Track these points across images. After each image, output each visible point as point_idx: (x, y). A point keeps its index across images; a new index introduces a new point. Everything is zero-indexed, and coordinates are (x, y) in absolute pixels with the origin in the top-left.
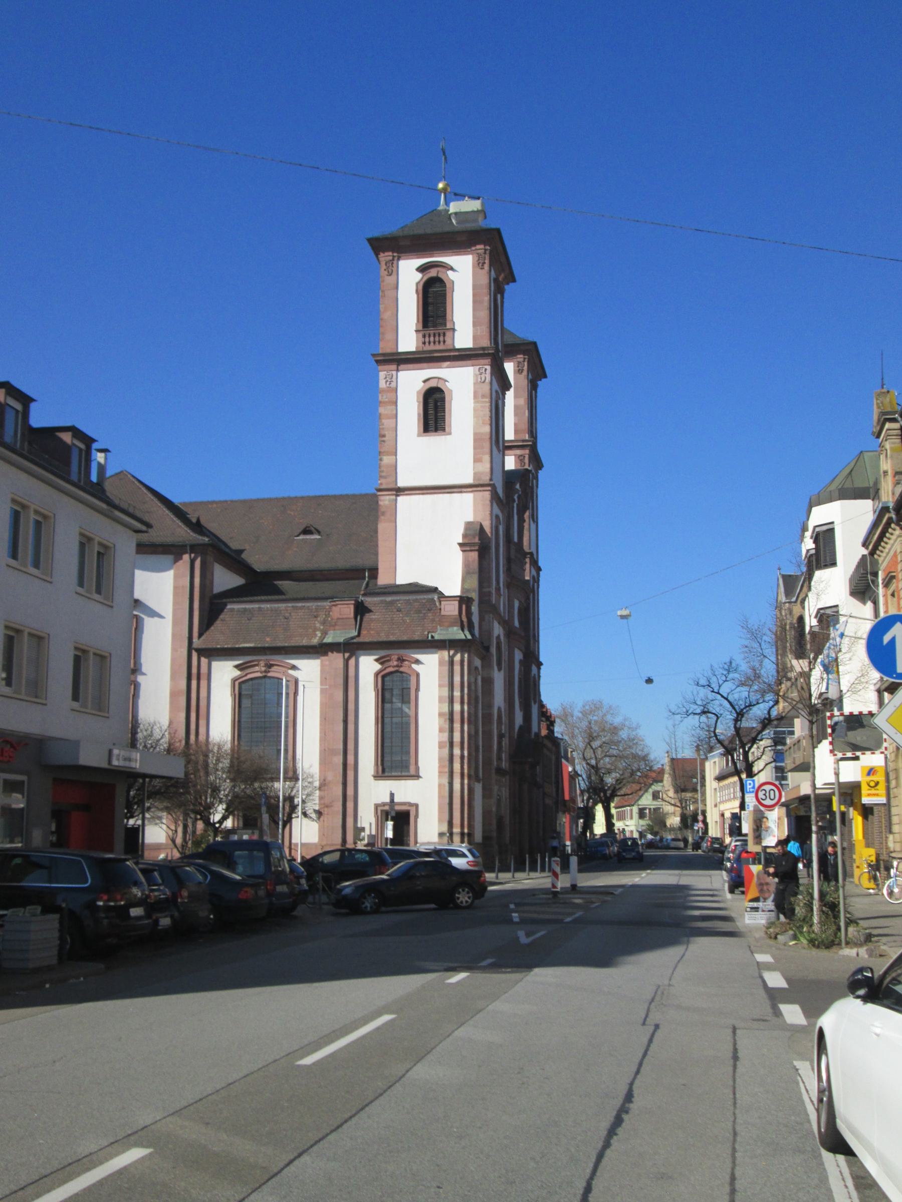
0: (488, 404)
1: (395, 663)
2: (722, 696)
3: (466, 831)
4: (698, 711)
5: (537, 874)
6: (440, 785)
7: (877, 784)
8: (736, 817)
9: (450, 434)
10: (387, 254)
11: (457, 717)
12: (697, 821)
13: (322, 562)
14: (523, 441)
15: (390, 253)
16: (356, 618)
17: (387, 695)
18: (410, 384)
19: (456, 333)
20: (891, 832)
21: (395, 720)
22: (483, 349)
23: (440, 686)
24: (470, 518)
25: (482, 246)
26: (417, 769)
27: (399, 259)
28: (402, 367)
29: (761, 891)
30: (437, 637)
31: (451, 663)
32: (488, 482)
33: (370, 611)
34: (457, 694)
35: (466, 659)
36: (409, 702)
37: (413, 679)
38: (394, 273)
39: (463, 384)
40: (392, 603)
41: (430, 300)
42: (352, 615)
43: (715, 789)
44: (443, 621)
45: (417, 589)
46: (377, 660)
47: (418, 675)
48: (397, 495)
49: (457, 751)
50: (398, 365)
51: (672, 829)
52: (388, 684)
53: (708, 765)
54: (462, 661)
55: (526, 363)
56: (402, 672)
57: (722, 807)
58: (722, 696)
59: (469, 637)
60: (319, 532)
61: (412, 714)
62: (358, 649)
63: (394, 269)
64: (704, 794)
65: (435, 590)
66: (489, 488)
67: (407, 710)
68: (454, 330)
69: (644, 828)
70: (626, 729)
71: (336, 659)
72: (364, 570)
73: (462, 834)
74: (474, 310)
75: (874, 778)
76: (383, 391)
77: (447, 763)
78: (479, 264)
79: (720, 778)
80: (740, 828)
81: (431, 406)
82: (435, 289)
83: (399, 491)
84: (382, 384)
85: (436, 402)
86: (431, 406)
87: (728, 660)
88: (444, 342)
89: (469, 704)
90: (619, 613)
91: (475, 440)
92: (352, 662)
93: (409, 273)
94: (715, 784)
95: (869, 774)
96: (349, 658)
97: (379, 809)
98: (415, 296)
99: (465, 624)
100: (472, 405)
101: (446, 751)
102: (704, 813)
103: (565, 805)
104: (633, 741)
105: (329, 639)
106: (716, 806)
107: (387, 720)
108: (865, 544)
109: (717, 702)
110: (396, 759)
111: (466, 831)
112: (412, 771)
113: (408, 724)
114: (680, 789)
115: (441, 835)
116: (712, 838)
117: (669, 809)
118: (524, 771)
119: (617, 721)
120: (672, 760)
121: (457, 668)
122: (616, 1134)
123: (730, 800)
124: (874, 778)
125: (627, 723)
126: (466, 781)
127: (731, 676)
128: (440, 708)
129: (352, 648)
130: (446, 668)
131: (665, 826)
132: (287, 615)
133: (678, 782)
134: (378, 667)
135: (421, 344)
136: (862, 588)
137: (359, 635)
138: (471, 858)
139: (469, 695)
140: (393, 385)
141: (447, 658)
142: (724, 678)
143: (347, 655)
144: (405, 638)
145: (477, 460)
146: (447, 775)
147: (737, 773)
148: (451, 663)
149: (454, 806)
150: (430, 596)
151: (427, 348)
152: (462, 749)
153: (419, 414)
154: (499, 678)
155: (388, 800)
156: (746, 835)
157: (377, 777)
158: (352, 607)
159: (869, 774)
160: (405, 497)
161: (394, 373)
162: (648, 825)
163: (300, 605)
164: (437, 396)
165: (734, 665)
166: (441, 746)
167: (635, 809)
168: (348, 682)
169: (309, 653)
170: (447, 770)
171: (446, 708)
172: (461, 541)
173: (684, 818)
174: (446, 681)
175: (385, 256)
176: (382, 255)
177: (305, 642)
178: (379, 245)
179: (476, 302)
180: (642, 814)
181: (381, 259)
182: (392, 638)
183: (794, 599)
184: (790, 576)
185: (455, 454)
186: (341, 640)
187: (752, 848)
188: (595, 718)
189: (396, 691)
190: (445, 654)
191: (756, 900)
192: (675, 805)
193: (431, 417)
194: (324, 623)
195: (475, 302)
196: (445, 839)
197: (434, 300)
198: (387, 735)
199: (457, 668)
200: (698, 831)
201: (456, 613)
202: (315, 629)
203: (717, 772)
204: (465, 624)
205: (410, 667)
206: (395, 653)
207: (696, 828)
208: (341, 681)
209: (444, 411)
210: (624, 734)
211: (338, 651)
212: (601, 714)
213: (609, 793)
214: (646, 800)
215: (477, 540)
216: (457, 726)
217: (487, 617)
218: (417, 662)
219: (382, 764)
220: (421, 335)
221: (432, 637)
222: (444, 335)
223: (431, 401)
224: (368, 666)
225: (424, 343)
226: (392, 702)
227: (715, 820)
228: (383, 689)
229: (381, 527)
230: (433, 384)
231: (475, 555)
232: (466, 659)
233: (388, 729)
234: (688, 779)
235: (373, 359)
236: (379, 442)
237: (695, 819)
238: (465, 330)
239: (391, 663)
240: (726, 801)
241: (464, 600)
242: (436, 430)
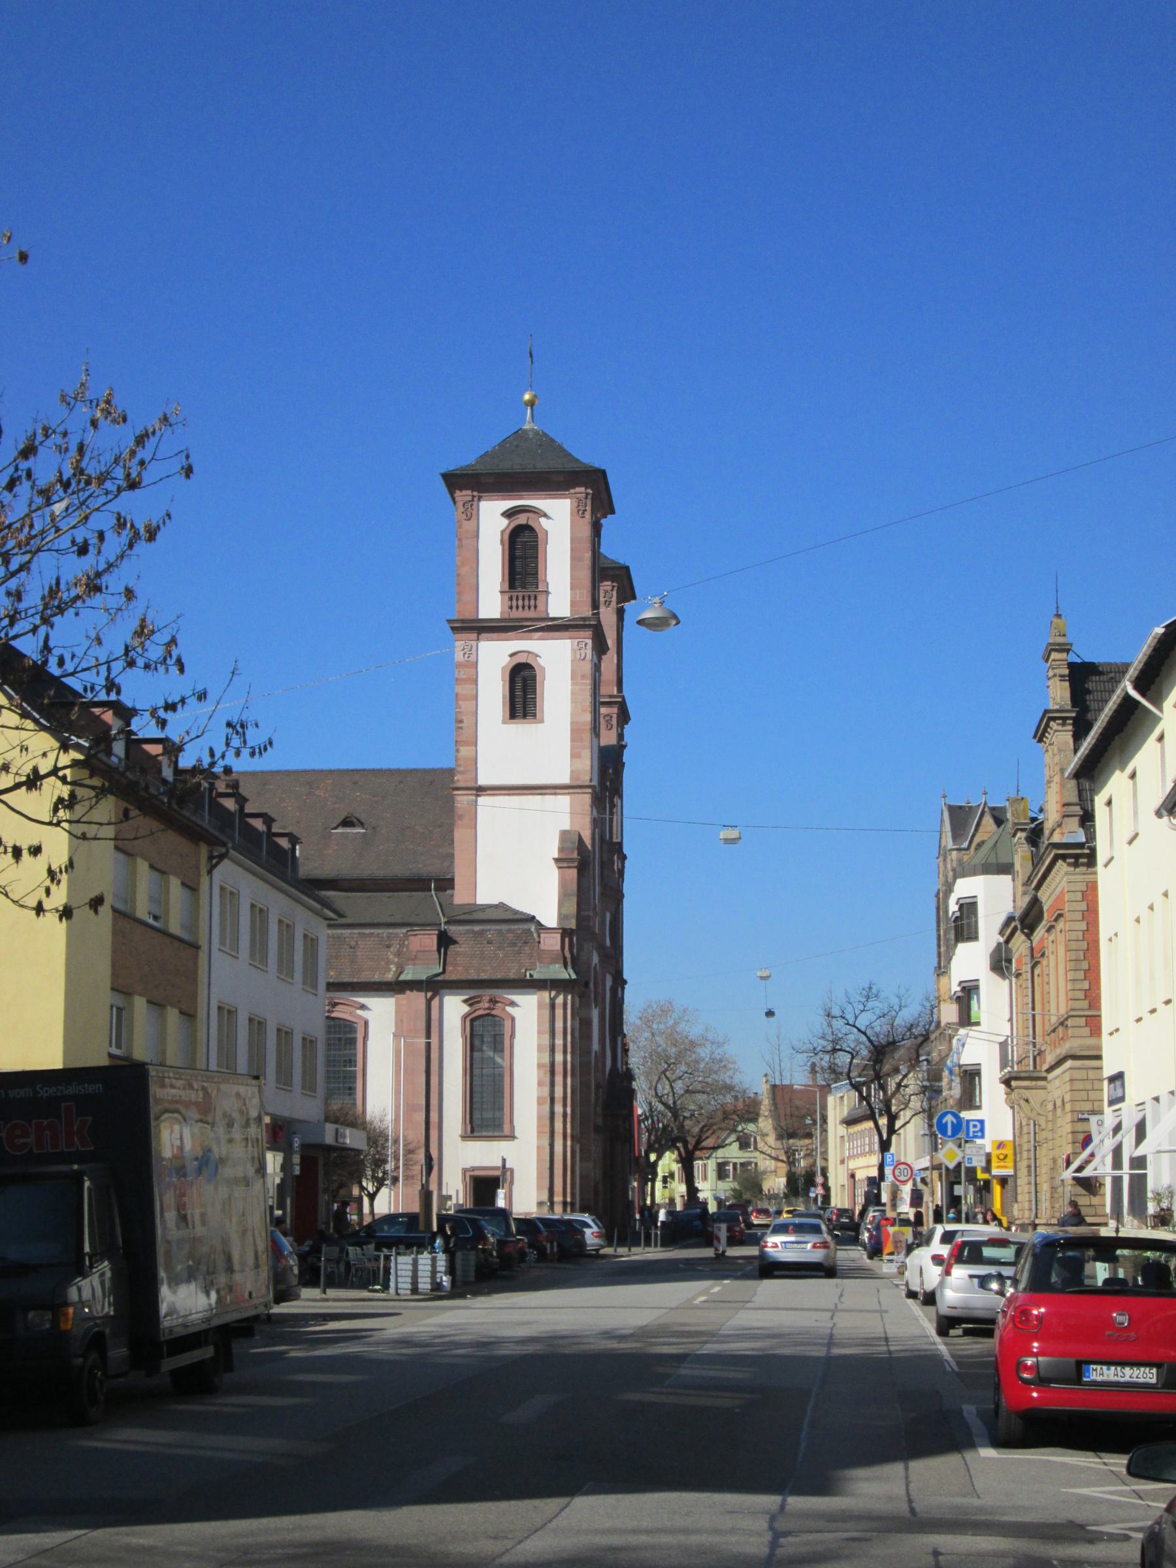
0: (589, 687)
1: (487, 1005)
2: (859, 1030)
3: (569, 1200)
4: (829, 1048)
5: (651, 1249)
6: (538, 1147)
7: (1006, 1156)
8: (874, 1183)
9: (542, 721)
10: (465, 492)
11: (559, 1068)
12: (814, 1185)
13: (371, 868)
14: (611, 696)
15: (469, 492)
16: (439, 951)
17: (477, 1043)
18: (494, 657)
19: (550, 597)
20: (1016, 1201)
21: (485, 1071)
22: (584, 619)
23: (539, 1032)
24: (567, 826)
25: (582, 489)
26: (512, 1128)
27: (480, 499)
28: (484, 635)
29: (896, 1247)
30: (536, 976)
31: (553, 1006)
32: (587, 783)
33: (455, 942)
34: (559, 1042)
35: (569, 1002)
36: (502, 1051)
37: (507, 1024)
38: (474, 517)
39: (558, 661)
40: (482, 932)
41: (518, 553)
42: (435, 947)
43: (842, 1137)
44: (542, 957)
45: (516, 917)
46: (465, 1001)
47: (513, 1019)
48: (478, 796)
49: (559, 1109)
50: (479, 634)
51: (772, 1197)
52: (479, 1030)
53: (831, 1100)
54: (565, 1004)
55: (615, 593)
56: (493, 1016)
57: (852, 1164)
58: (859, 1030)
59: (574, 976)
60: (362, 825)
61: (506, 1064)
62: (442, 988)
63: (474, 513)
64: (824, 1142)
65: (532, 919)
66: (590, 790)
67: (499, 1060)
68: (547, 593)
69: (728, 1194)
70: (708, 1045)
71: (417, 999)
72: (430, 880)
73: (565, 1203)
74: (573, 568)
75: (1004, 1151)
76: (459, 665)
77: (548, 1122)
78: (578, 512)
79: (850, 1122)
80: (878, 1196)
81: (519, 685)
82: (525, 537)
83: (481, 790)
84: (459, 656)
85: (525, 680)
86: (519, 685)
87: (866, 986)
88: (535, 607)
89: (572, 1053)
90: (759, 974)
91: (573, 731)
92: (435, 1003)
93: (492, 516)
94: (842, 1130)
95: (999, 1147)
96: (432, 998)
97: (468, 1174)
98: (500, 547)
99: (569, 960)
100: (570, 687)
101: (547, 1107)
102: (824, 1172)
103: (637, 1164)
104: (721, 1064)
105: (407, 976)
106: (842, 1162)
107: (476, 1072)
108: (1001, 933)
109: (852, 1037)
110: (487, 1114)
111: (569, 1200)
112: (506, 1131)
113: (501, 1076)
114: (786, 1134)
115: (540, 1204)
116: (839, 1210)
117: (765, 1164)
118: (607, 1120)
119: (695, 1032)
120: (774, 1087)
121: (559, 1012)
122: (1089, 692)
123: (863, 1154)
124: (1004, 1151)
125: (710, 1036)
126: (569, 1143)
127: (870, 1005)
128: (539, 1059)
129: (435, 987)
130: (546, 1013)
131: (761, 1190)
132: (353, 943)
133: (783, 1123)
134: (466, 1009)
135: (507, 609)
136: (1000, 963)
137: (444, 972)
138: (595, 1229)
139: (572, 1042)
140: (473, 658)
141: (547, 1000)
142: (861, 1007)
143: (429, 994)
144: (499, 976)
145: (574, 755)
146: (547, 1136)
147: (872, 1117)
148: (553, 1006)
149: (556, 1171)
150: (525, 926)
151: (516, 614)
152: (565, 1106)
153: (504, 696)
154: (595, 1014)
155: (500, 1164)
156: (884, 1205)
157: (464, 1137)
158: (435, 938)
159: (999, 1147)
160: (487, 798)
161: (474, 643)
162: (734, 1190)
163: (368, 931)
164: (526, 673)
165: (874, 991)
166: (540, 1102)
167: (711, 1165)
168: (431, 1026)
169: (382, 990)
170: (547, 1129)
171: (546, 1059)
172: (556, 856)
173: (791, 1179)
174: (547, 1026)
175: (463, 496)
176: (458, 493)
177: (377, 978)
178: (455, 481)
179: (575, 558)
180: (721, 1173)
181: (457, 499)
182: (484, 976)
183: (965, 845)
184: (961, 807)
185: (550, 748)
186: (424, 978)
187: (890, 1214)
188: (662, 1026)
189: (487, 1037)
190: (546, 995)
191: (892, 1254)
192: (776, 1159)
193: (519, 700)
194: (399, 954)
195: (573, 558)
196: (546, 1209)
197: (523, 549)
198: (476, 1089)
199: (559, 1012)
200: (816, 1199)
201: (558, 947)
202: (388, 962)
203: (846, 1113)
204: (569, 960)
205: (504, 1009)
206: (487, 993)
207: (812, 1195)
208: (422, 1024)
209: (535, 692)
210: (703, 1052)
211: (419, 990)
212: (671, 1022)
213: (692, 1141)
214: (732, 1152)
215: (575, 855)
216: (559, 1079)
217: (586, 946)
218: (513, 1004)
219: (471, 1122)
220: (507, 597)
221: (531, 976)
222: (535, 599)
223: (519, 679)
224: (454, 1007)
225: (511, 608)
226: (481, 1050)
227: (840, 1182)
228: (472, 1035)
229: (459, 834)
230: (521, 659)
231: (573, 873)
232: (569, 1002)
233: (476, 1082)
234: (798, 1119)
235: (447, 627)
236: (464, 732)
237: (810, 1180)
238: (561, 593)
239: (481, 1005)
240: (858, 1155)
241: (565, 933)
242: (525, 716)
